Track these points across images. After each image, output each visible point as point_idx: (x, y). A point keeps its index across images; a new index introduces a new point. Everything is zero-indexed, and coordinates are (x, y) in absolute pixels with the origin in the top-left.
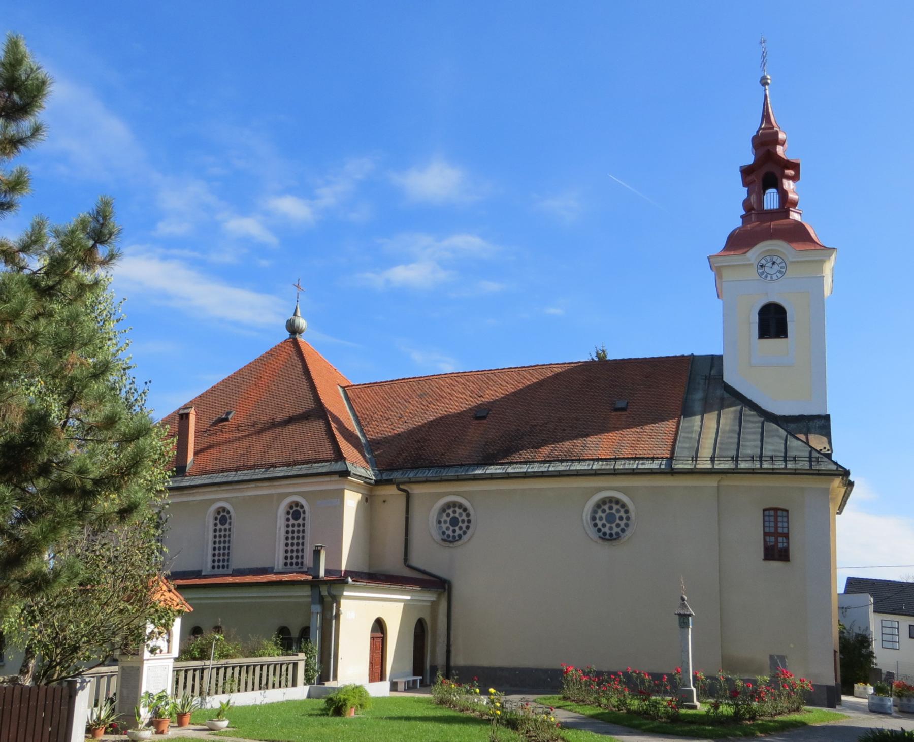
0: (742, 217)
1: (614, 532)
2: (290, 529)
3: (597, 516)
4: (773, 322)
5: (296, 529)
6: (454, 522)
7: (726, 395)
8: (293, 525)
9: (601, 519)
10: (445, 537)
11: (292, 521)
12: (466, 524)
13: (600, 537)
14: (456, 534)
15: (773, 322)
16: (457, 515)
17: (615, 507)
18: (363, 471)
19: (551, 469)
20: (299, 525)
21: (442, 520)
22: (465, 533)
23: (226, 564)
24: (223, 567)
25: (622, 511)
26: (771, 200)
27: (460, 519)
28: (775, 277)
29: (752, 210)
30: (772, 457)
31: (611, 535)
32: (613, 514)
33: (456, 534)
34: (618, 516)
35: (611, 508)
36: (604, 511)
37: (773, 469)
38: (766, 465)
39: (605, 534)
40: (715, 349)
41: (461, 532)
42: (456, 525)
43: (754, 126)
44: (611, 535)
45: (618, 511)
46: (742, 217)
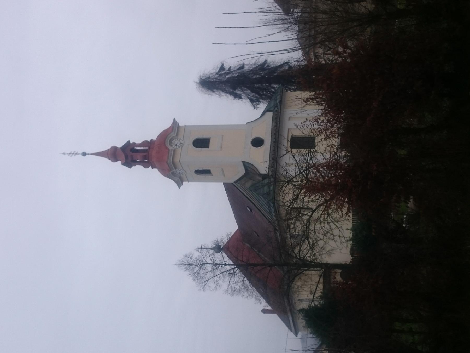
43: (106, 161)
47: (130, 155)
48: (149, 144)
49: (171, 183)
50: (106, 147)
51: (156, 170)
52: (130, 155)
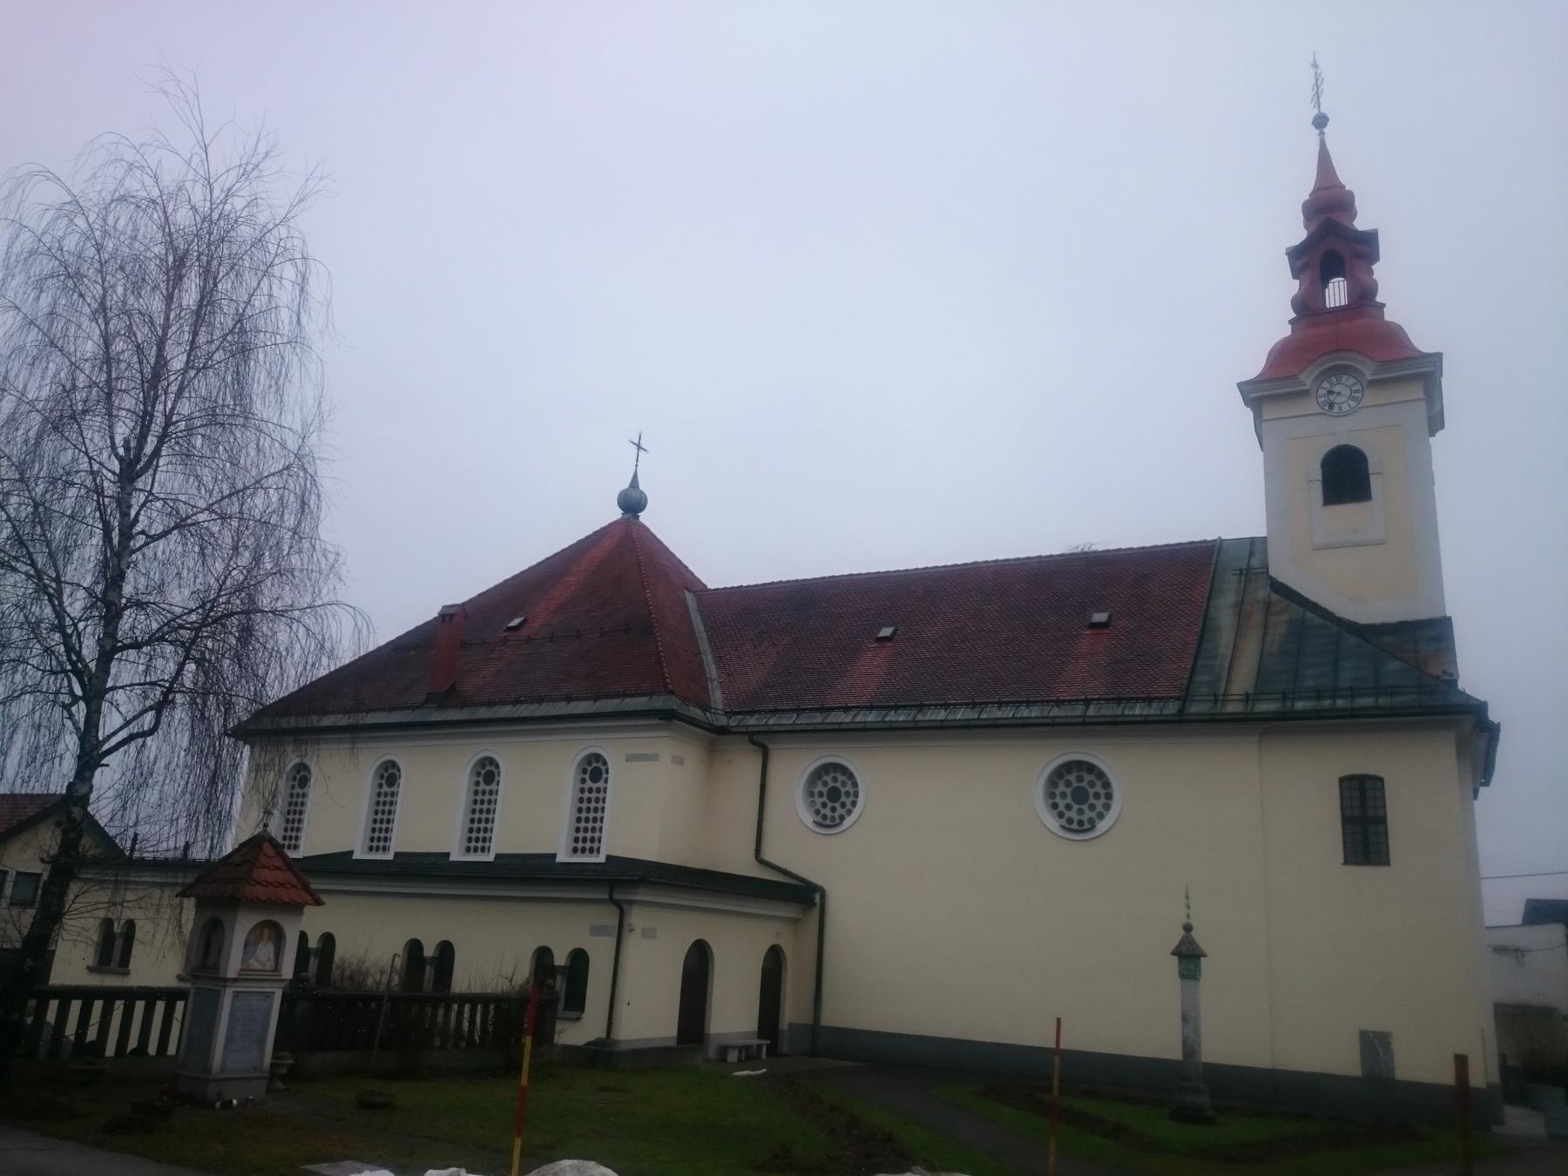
0: (1291, 322)
1: (1084, 818)
2: (586, 795)
3: (1057, 792)
4: (1345, 477)
5: (594, 795)
6: (834, 795)
7: (1275, 597)
8: (590, 790)
9: (1064, 795)
10: (819, 819)
11: (589, 784)
12: (1061, 808)
13: (1063, 827)
14: (836, 815)
15: (1345, 477)
16: (838, 785)
17: (1087, 777)
18: (699, 712)
19: (984, 716)
20: (598, 790)
21: (816, 791)
22: (849, 812)
23: (595, 845)
24: (591, 851)
25: (1099, 784)
26: (1337, 293)
27: (843, 790)
28: (1345, 408)
29: (1308, 309)
30: (1351, 689)
31: (1081, 823)
32: (1083, 789)
33: (836, 815)
34: (1091, 791)
35: (1080, 779)
36: (1068, 784)
37: (1353, 709)
38: (1340, 703)
39: (1070, 821)
40: (1264, 534)
41: (1093, 815)
42: (833, 796)
43: (1304, 185)
44: (1081, 823)
45: (1092, 784)
46: (1291, 322)
47: (1333, 244)
48: (1364, 298)
49: (1254, 366)
50: (1347, 176)
51: (1287, 331)
52: (1333, 244)
